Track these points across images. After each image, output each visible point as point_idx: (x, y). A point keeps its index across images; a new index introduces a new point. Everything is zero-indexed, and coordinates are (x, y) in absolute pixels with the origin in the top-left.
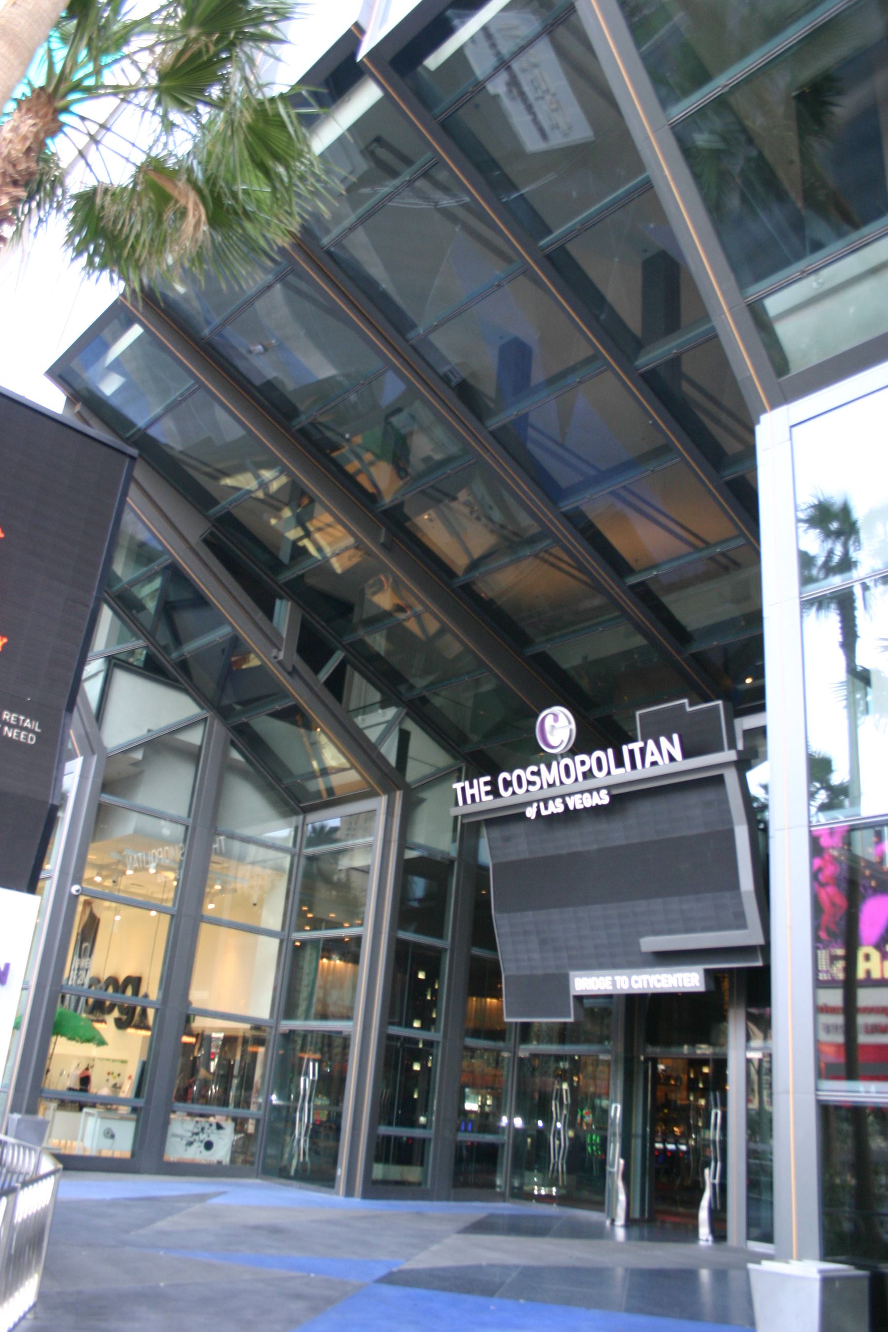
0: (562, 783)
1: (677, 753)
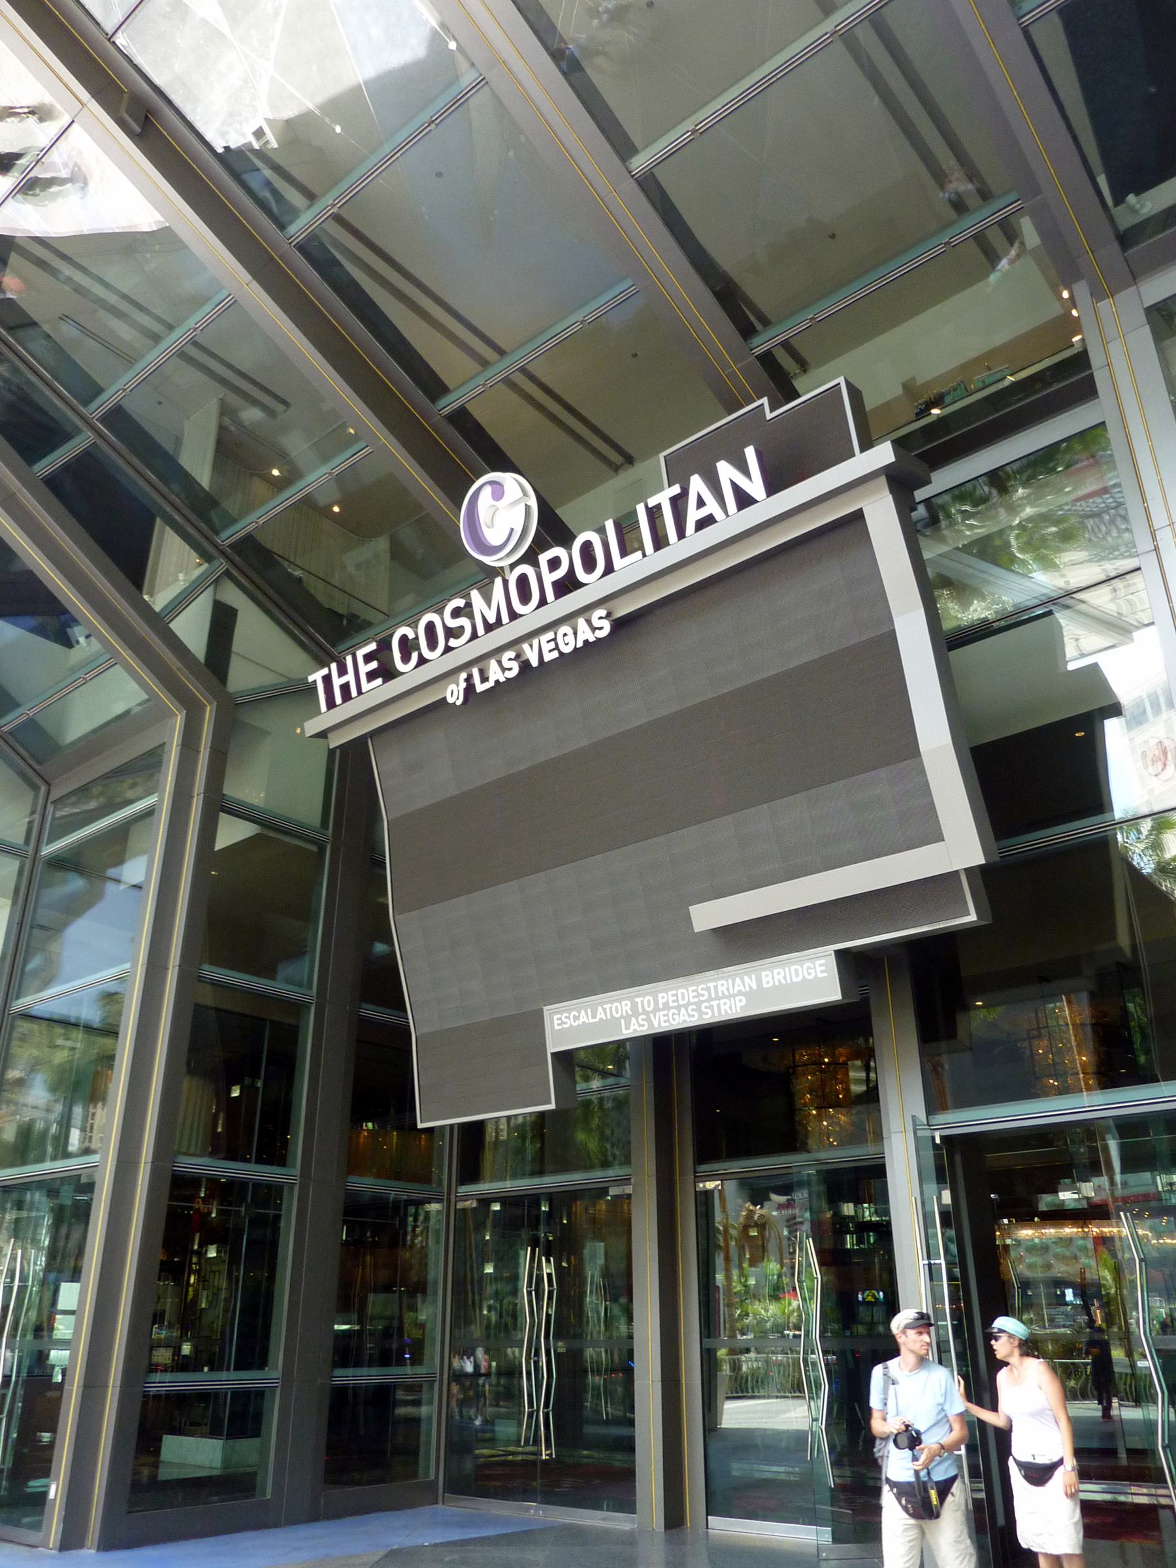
0: (513, 616)
1: (755, 487)
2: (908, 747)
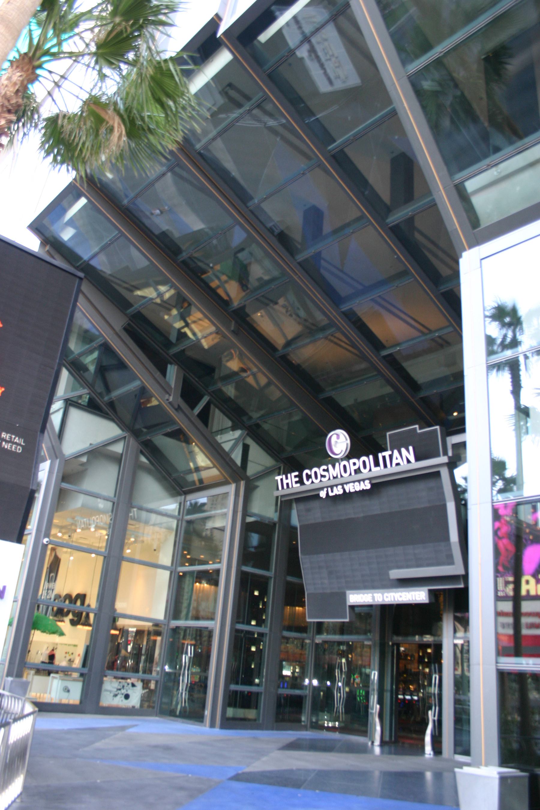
0: (341, 476)
1: (412, 458)
2: (446, 537)
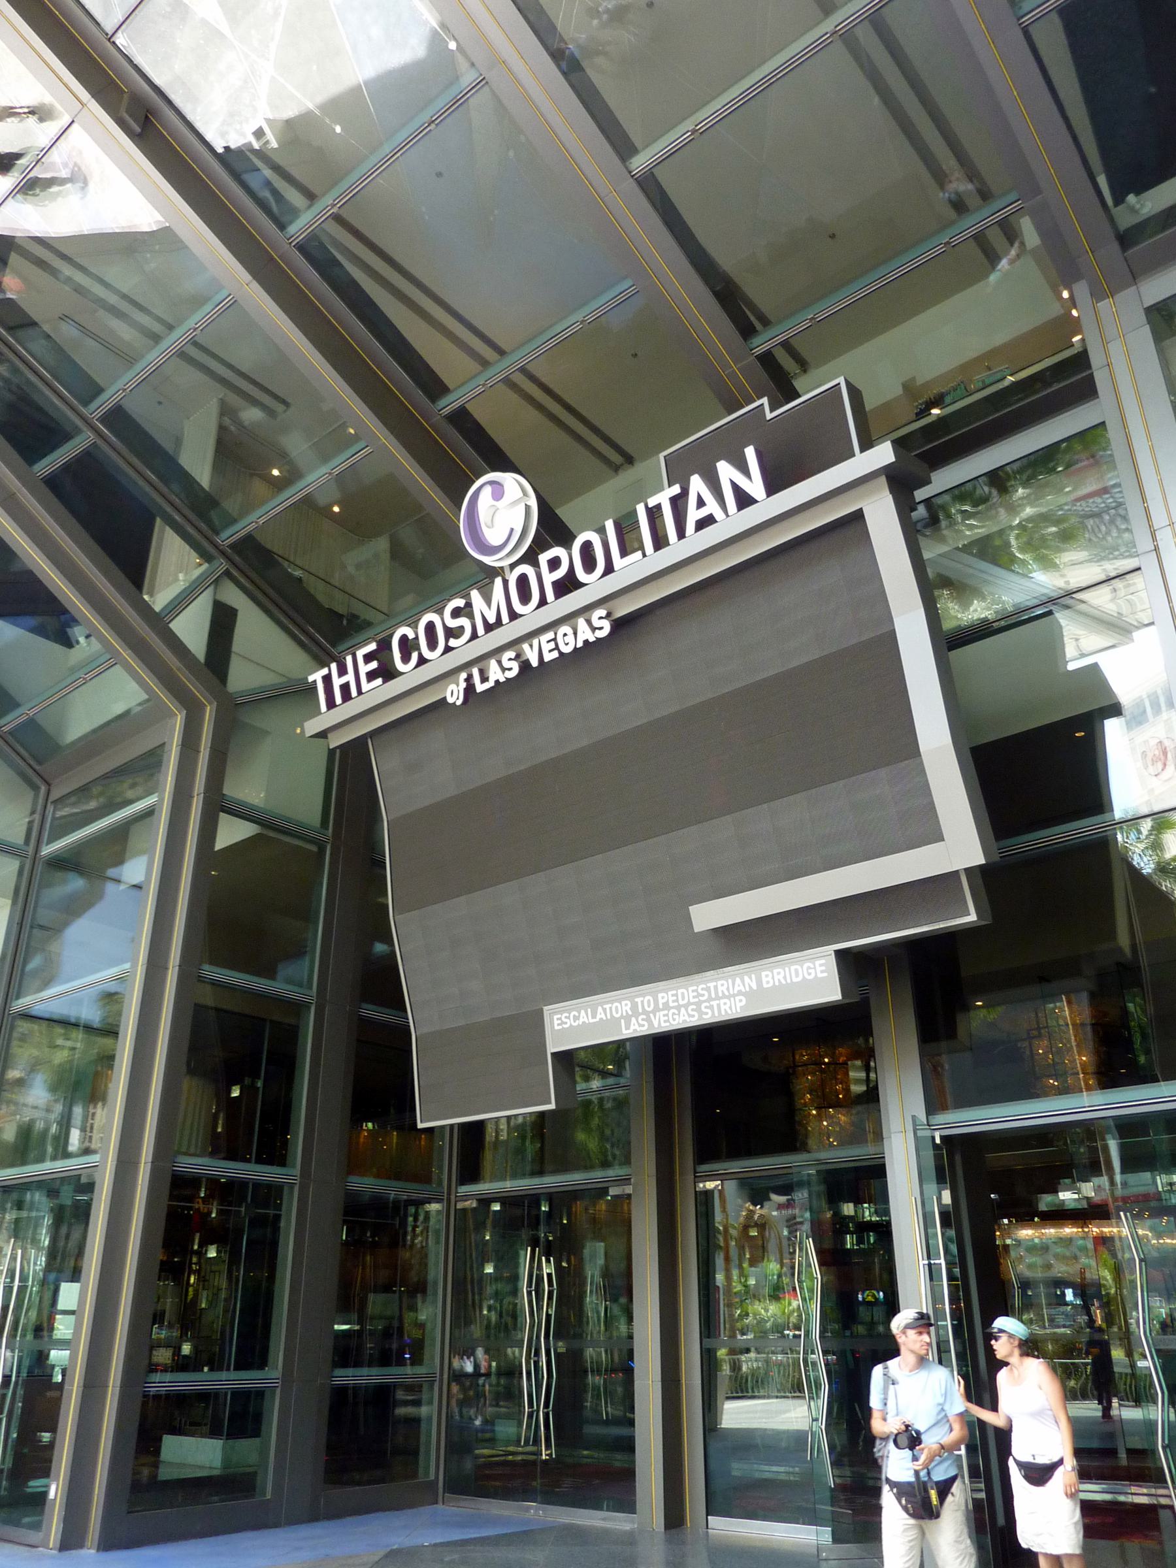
0: (513, 616)
1: (755, 487)
